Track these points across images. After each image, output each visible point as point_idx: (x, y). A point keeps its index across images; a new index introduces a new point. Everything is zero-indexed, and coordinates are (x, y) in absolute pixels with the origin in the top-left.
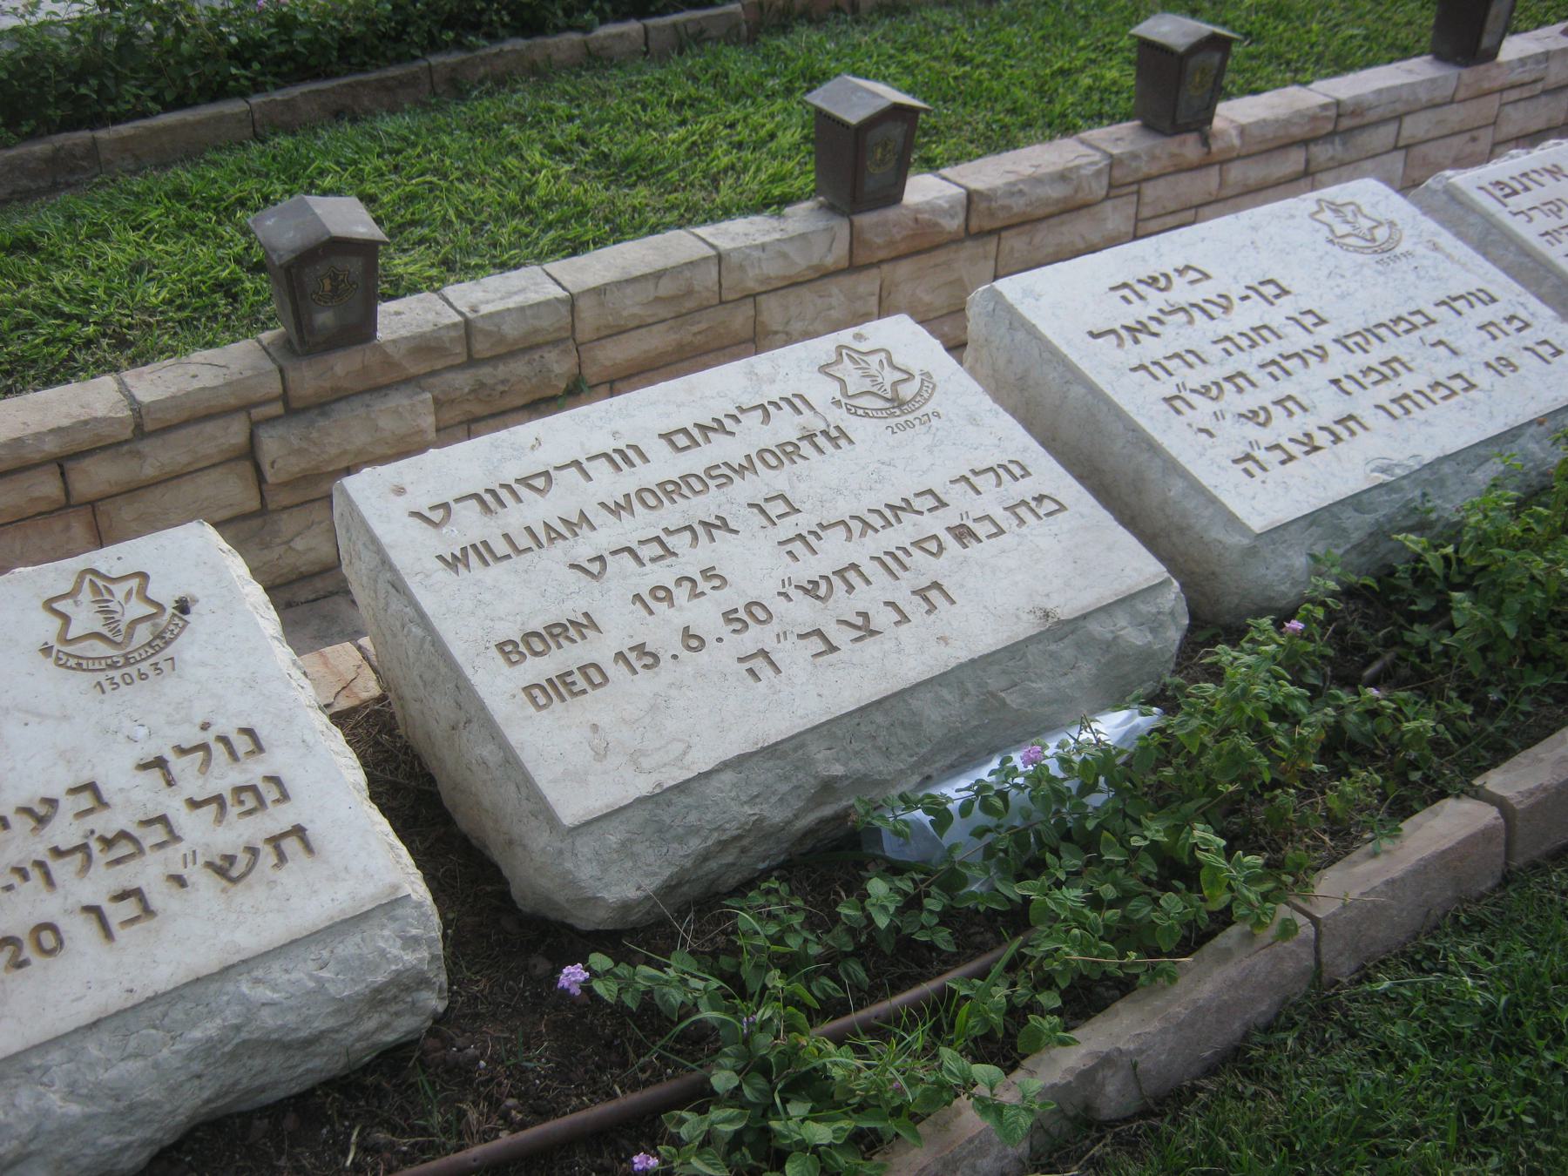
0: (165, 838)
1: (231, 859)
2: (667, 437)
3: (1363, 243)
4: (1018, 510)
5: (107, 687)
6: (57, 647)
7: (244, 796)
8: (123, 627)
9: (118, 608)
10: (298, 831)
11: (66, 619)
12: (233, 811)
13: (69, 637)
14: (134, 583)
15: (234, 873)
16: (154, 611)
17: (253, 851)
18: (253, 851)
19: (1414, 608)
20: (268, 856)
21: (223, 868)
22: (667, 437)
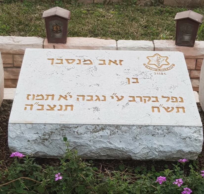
0: (132, 100)
1: (169, 108)
2: (67, 60)
3: (156, 68)
4: (179, 109)
5: (159, 74)
6: (147, 64)
7: (174, 99)
8: (161, 65)
9: (161, 61)
10: (183, 108)
11: (150, 61)
12: (171, 100)
13: (150, 63)
14: (166, 58)
15: (168, 110)
16: (167, 64)
17: (173, 108)
18: (173, 108)
19: (56, 180)
20: (175, 110)
21: (167, 109)
22: (67, 60)
